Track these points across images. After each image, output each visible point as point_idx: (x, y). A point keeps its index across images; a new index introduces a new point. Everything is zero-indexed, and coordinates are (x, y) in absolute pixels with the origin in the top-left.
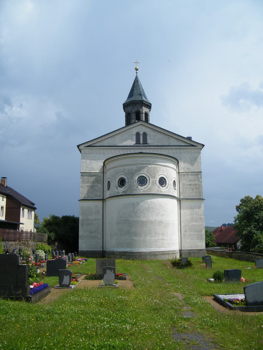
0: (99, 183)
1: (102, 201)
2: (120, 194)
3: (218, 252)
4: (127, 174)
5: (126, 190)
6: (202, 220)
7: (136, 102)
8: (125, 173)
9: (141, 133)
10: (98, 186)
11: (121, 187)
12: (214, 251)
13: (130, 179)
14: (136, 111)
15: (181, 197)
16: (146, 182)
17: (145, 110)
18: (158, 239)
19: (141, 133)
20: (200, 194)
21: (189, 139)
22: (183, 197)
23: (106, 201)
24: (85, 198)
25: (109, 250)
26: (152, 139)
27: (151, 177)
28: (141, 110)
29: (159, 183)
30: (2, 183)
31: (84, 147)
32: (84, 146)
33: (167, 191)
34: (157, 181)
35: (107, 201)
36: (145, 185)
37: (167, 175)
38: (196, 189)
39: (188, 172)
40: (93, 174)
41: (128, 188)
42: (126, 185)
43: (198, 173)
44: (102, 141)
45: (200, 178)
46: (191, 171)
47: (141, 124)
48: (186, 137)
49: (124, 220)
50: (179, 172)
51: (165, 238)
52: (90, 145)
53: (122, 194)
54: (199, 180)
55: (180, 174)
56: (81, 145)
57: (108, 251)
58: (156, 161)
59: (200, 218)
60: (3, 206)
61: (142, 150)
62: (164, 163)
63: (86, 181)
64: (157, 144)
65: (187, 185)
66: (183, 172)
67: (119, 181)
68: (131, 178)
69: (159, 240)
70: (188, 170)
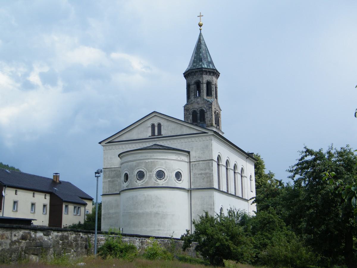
2: (125, 189)
4: (129, 170)
5: (128, 185)
7: (194, 71)
9: (156, 125)
10: (117, 181)
11: (140, 180)
14: (196, 82)
15: (192, 187)
17: (206, 78)
18: (154, 230)
19: (156, 125)
20: (211, 183)
22: (194, 187)
24: (107, 193)
26: (165, 130)
27: (148, 171)
28: (201, 80)
30: (54, 179)
32: (104, 143)
33: (165, 183)
34: (154, 175)
37: (166, 167)
38: (207, 178)
39: (199, 161)
40: (113, 169)
41: (129, 183)
43: (209, 161)
44: (121, 137)
45: (211, 166)
46: (202, 160)
50: (190, 162)
51: (161, 228)
52: (109, 142)
54: (209, 169)
55: (191, 163)
58: (153, 156)
59: (210, 208)
60: (33, 203)
62: (162, 156)
63: (107, 176)
65: (198, 174)
66: (195, 162)
69: (155, 231)
70: (199, 159)
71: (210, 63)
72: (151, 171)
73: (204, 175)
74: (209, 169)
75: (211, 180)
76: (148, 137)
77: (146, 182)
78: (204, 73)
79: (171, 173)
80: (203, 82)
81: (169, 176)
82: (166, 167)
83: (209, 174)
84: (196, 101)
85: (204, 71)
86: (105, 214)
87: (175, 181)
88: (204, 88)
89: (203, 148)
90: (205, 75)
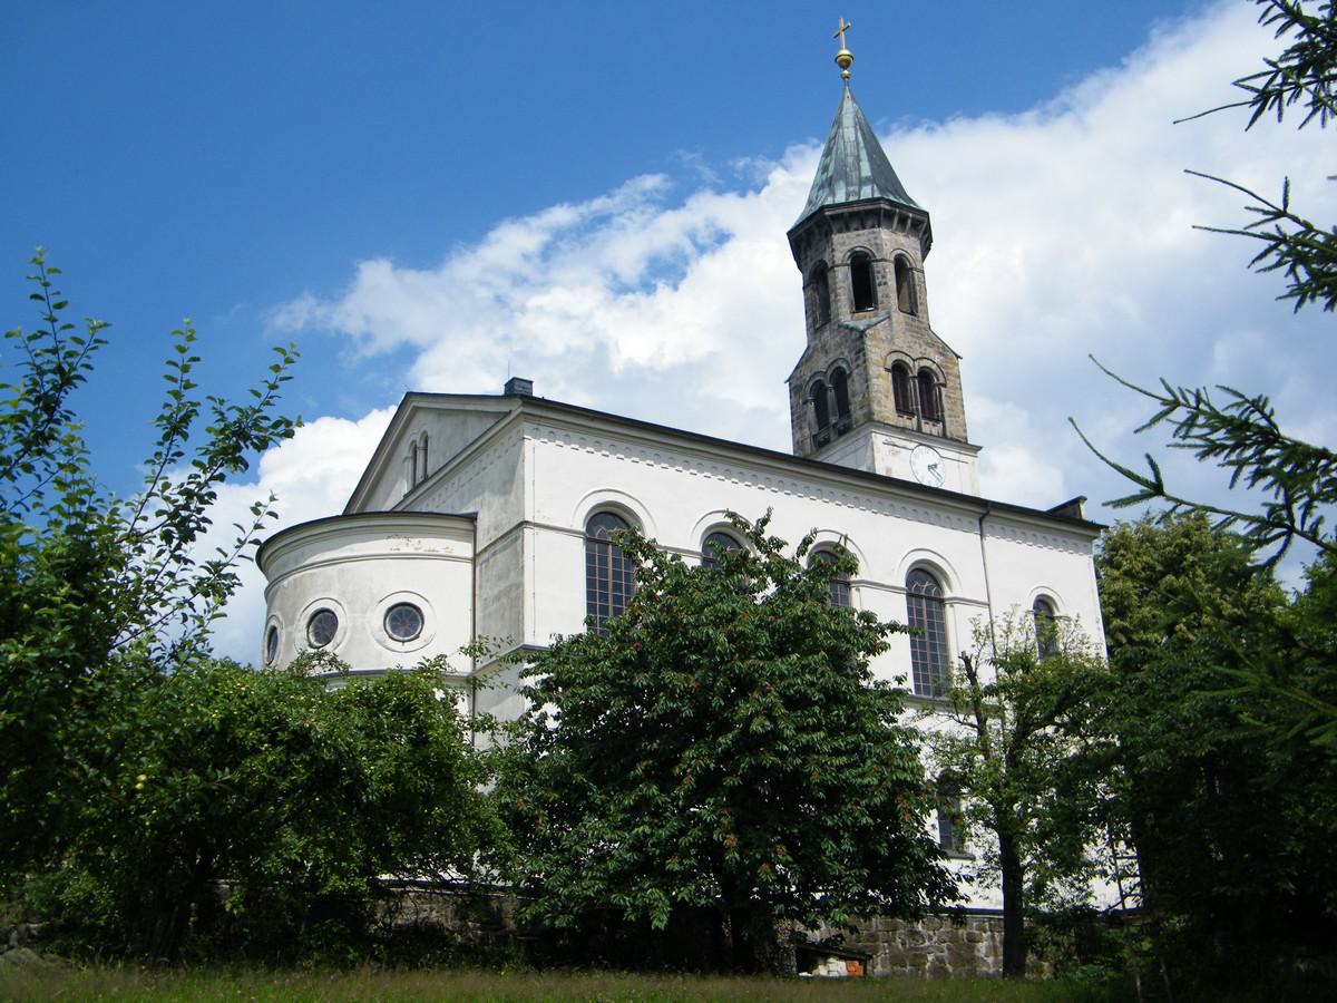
37: (343, 593)
71: (1301, 263)
79: (364, 612)
80: (834, 262)
81: (354, 627)
82: (343, 593)
84: (820, 346)
85: (831, 216)
87: (380, 642)
88: (840, 284)
90: (840, 231)
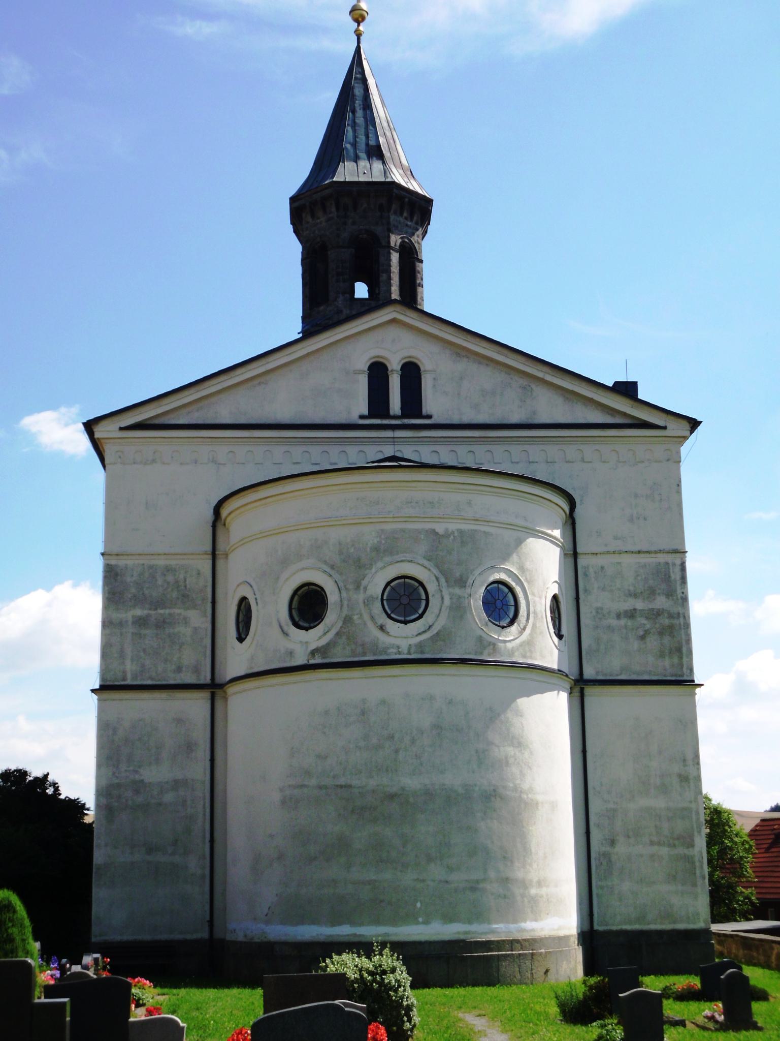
0: (194, 607)
1: (205, 695)
3: (772, 949)
4: (332, 567)
5: (328, 644)
6: (692, 784)
8: (325, 562)
9: (395, 365)
10: (186, 621)
11: (307, 629)
12: (753, 939)
13: (347, 589)
16: (423, 604)
19: (395, 365)
20: (681, 658)
21: (627, 389)
23: (225, 692)
25: (245, 936)
29: (485, 603)
31: (121, 429)
33: (521, 645)
35: (234, 694)
36: (421, 617)
38: (661, 633)
42: (331, 617)
45: (679, 583)
47: (394, 321)
48: (611, 385)
49: (320, 787)
53: (312, 662)
54: (670, 594)
56: (230, 500)
57: (241, 938)
59: (680, 776)
61: (397, 447)
64: (469, 417)
67: (296, 598)
68: (351, 587)
72: (462, 582)
73: (647, 618)
74: (670, 594)
75: (680, 643)
76: (354, 418)
77: (437, 634)
78: (394, 207)
83: (671, 616)
86: (119, 786)
89: (636, 496)
